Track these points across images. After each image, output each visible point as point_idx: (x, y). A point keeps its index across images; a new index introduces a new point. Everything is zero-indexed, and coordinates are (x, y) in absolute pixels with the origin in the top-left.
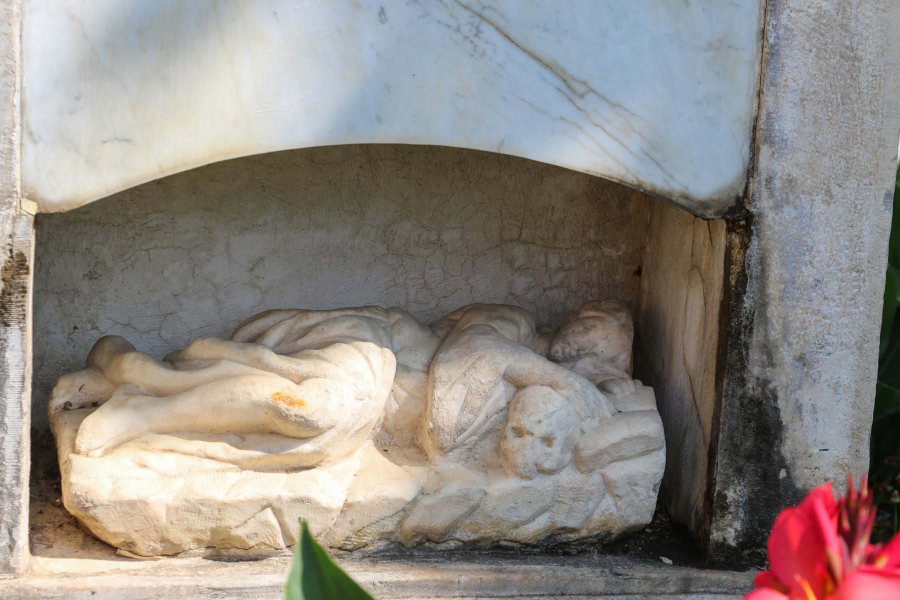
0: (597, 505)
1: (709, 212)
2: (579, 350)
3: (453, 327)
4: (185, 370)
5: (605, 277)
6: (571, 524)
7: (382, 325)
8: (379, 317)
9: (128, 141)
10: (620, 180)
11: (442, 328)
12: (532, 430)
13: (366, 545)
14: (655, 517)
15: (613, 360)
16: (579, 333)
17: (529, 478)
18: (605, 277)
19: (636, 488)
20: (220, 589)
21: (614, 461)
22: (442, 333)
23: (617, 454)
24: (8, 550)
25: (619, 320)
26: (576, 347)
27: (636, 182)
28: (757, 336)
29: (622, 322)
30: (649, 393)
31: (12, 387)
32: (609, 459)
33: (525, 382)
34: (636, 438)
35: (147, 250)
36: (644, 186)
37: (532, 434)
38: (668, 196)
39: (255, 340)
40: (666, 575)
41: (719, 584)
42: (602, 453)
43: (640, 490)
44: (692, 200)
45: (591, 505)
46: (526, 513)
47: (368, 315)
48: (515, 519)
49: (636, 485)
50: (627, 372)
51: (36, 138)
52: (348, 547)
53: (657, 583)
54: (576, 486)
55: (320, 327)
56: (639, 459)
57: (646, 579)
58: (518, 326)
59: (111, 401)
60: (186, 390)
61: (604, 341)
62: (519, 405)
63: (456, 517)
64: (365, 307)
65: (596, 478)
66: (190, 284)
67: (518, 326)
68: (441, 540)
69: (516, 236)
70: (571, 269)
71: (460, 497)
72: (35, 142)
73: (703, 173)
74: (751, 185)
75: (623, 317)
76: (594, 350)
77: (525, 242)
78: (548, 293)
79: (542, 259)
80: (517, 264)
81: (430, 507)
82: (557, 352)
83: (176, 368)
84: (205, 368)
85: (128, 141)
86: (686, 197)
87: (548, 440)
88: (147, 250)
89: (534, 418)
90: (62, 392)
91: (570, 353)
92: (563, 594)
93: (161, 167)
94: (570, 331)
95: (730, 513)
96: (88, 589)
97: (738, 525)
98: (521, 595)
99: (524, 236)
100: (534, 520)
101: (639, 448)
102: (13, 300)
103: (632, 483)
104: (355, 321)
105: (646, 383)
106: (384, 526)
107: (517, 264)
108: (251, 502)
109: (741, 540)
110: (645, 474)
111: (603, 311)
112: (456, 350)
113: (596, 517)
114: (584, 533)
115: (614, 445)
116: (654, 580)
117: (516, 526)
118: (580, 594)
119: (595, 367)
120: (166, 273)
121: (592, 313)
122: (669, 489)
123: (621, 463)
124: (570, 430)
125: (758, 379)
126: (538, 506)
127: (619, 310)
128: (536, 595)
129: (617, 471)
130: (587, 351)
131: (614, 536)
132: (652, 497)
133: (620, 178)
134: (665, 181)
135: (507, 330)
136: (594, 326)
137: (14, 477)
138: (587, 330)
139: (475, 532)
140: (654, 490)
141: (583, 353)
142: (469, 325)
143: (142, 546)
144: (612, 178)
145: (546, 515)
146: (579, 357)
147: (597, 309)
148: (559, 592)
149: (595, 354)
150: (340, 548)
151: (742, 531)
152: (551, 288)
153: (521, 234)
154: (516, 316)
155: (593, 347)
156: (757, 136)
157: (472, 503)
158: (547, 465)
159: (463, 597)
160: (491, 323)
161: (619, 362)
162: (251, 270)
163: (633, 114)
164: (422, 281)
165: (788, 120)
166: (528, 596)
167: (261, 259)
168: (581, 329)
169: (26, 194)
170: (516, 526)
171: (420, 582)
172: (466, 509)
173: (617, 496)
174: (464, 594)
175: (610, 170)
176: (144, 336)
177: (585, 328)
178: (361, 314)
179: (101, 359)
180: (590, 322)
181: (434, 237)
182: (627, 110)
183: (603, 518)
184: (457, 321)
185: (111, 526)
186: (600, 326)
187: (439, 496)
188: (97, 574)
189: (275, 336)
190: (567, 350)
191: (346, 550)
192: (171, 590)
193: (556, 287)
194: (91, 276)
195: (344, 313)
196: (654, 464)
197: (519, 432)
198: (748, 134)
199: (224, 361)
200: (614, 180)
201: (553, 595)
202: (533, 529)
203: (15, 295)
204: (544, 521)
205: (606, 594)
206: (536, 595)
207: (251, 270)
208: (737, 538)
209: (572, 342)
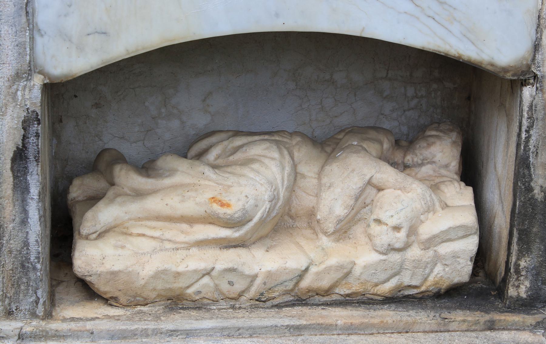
0: (432, 271)
1: (508, 74)
2: (423, 160)
3: (337, 144)
4: (153, 178)
5: (446, 102)
6: (414, 283)
7: (287, 146)
8: (285, 140)
9: (105, 33)
10: (446, 54)
11: (329, 145)
12: (386, 222)
13: (274, 298)
14: (474, 274)
15: (446, 166)
16: (424, 148)
17: (385, 254)
18: (446, 102)
19: (458, 260)
20: (174, 331)
21: (443, 242)
22: (328, 149)
23: (445, 237)
24: (35, 304)
25: (451, 138)
26: (421, 157)
27: (457, 55)
28: (541, 159)
29: (454, 139)
30: (469, 191)
31: (32, 199)
32: (440, 241)
33: (383, 187)
34: (458, 227)
35: (133, 89)
36: (463, 57)
37: (387, 225)
38: (479, 64)
39: (199, 156)
40: (477, 318)
41: (514, 323)
42: (435, 237)
43: (461, 261)
44: (496, 67)
45: (427, 271)
46: (383, 277)
47: (277, 138)
48: (376, 281)
49: (458, 257)
50: (456, 173)
51: (43, 33)
52: (263, 299)
53: (471, 324)
54: (417, 258)
55: (244, 148)
56: (461, 240)
57: (464, 321)
58: (381, 144)
59: (104, 199)
60: (154, 192)
61: (441, 154)
62: (378, 204)
63: (336, 280)
64: (277, 132)
65: (431, 253)
66: (163, 110)
67: (381, 144)
68: (325, 294)
69: (384, 75)
70: (422, 97)
71: (338, 266)
72: (42, 36)
74: (537, 56)
75: (454, 135)
76: (434, 160)
77: (390, 79)
78: (407, 113)
79: (403, 90)
80: (385, 94)
81: (318, 274)
82: (408, 160)
83: (148, 176)
84: (167, 177)
85: (105, 33)
86: (492, 65)
87: (397, 228)
88: (133, 89)
89: (389, 214)
90: (75, 189)
91: (417, 162)
92: (407, 332)
93: (127, 50)
94: (418, 146)
95: (522, 276)
96: (88, 331)
97: (527, 284)
98: (379, 333)
99: (389, 75)
100: (389, 280)
101: (461, 234)
102: (30, 141)
103: (455, 256)
104: (268, 144)
105: (467, 184)
106: (286, 286)
107: (385, 94)
108: (195, 271)
109: (529, 293)
110: (465, 250)
111: (441, 131)
112: (337, 164)
113: (431, 278)
114: (423, 288)
115: (443, 232)
116: (469, 322)
117: (376, 285)
118: (419, 332)
119: (434, 171)
120: (147, 104)
121: (434, 133)
122: (482, 258)
123: (448, 244)
124: (413, 221)
125: (541, 187)
126: (390, 272)
127: (452, 131)
128: (389, 333)
129: (445, 249)
130: (428, 160)
131: (443, 291)
132: (469, 265)
133: (446, 52)
134: (478, 54)
135: (373, 148)
136: (434, 143)
137: (36, 257)
138: (429, 145)
139: (349, 289)
140: (471, 260)
141: (426, 161)
142: (347, 145)
143: (123, 300)
144: (441, 52)
145: (397, 277)
146: (422, 165)
147: (437, 130)
148: (405, 331)
149: (434, 162)
150: (257, 300)
151: (530, 287)
152: (409, 110)
153: (387, 73)
154: (382, 137)
155: (433, 158)
157: (345, 271)
158: (397, 245)
159: (339, 334)
160: (362, 144)
161: (451, 167)
162: (204, 101)
163: (455, 9)
164: (320, 106)
166: (383, 333)
167: (210, 93)
168: (425, 145)
169: (37, 71)
170: (376, 285)
171: (310, 325)
172: (342, 275)
173: (445, 265)
174: (340, 332)
175: (439, 47)
176: (134, 145)
177: (428, 144)
178: (273, 138)
179: (102, 166)
180: (432, 140)
181: (328, 77)
182: (450, 6)
183: (436, 279)
184: (341, 139)
185: (102, 287)
186: (438, 143)
187: (323, 267)
188: (93, 319)
189: (211, 156)
190: (415, 159)
191: (261, 301)
192: (142, 331)
193: (413, 109)
194: (97, 105)
195: (262, 137)
196: (471, 244)
197: (378, 221)
198: (535, 20)
199: (179, 173)
200: (442, 54)
201: (400, 333)
202: (387, 288)
203: (32, 138)
204: (396, 281)
205: (437, 332)
206: (389, 333)
207: (204, 101)
208: (527, 292)
209: (418, 154)
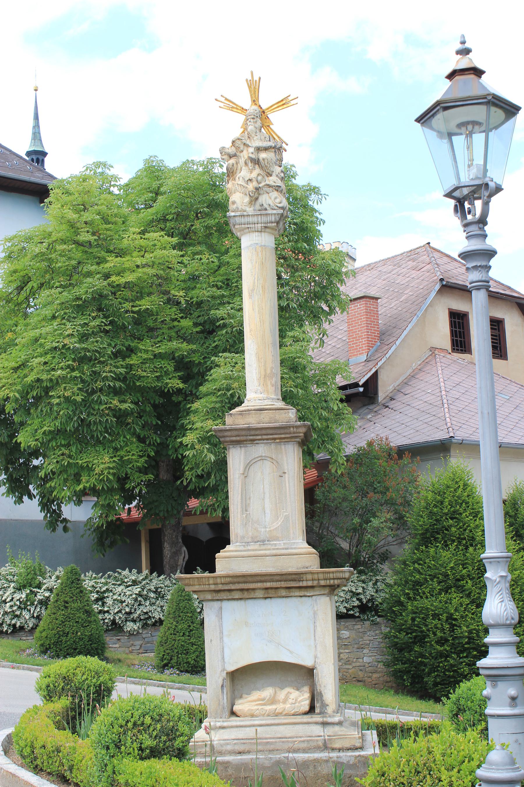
73: (308, 663)
156: (316, 657)
165: (319, 655)
